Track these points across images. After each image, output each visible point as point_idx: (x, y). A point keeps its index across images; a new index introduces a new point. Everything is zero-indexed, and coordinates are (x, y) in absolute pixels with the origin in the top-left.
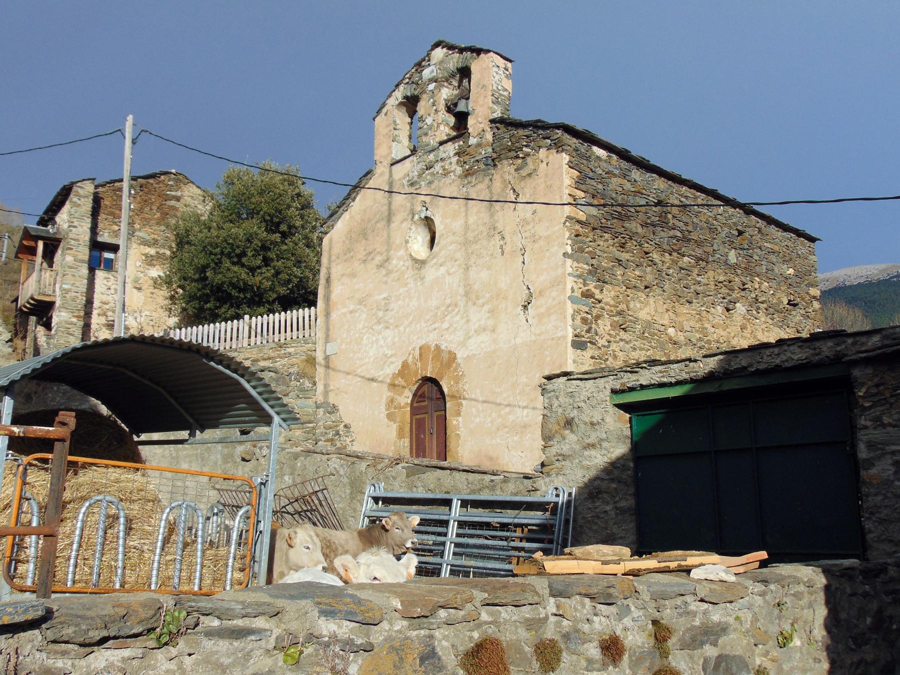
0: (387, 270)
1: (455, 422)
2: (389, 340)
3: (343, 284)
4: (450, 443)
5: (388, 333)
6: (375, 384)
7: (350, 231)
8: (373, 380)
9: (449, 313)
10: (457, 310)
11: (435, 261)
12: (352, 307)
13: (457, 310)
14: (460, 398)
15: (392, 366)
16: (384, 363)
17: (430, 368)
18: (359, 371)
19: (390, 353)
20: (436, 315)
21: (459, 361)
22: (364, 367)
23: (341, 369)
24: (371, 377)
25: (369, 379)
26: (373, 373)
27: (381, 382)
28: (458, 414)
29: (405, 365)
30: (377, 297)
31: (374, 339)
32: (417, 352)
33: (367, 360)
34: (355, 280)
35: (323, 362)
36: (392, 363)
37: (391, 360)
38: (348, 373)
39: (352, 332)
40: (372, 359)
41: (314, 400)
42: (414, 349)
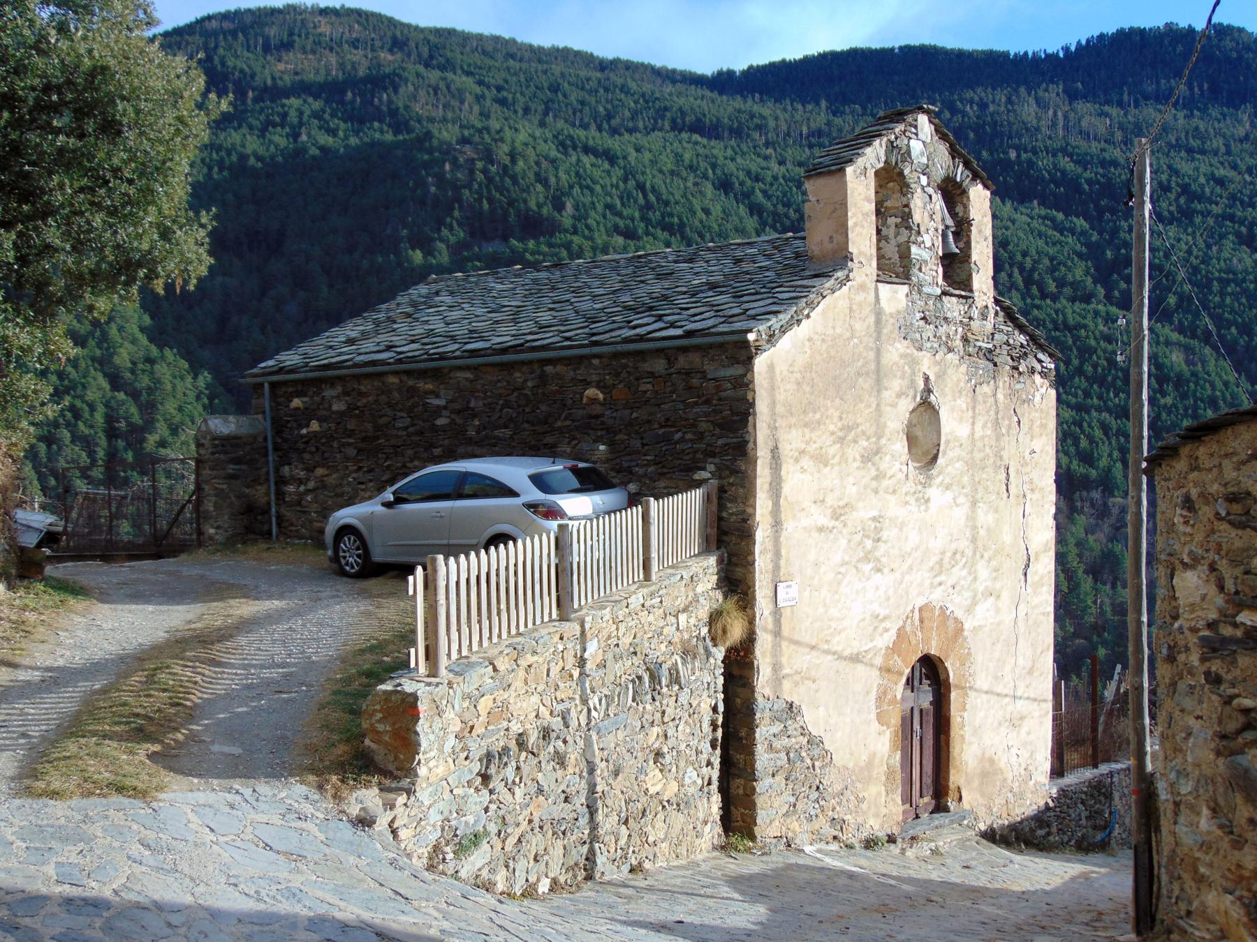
0: (878, 469)
1: (959, 719)
3: (803, 470)
11: (941, 478)
13: (964, 560)
15: (886, 635)
17: (934, 643)
20: (940, 563)
22: (843, 635)
29: (901, 633)
36: (886, 630)
37: (884, 625)
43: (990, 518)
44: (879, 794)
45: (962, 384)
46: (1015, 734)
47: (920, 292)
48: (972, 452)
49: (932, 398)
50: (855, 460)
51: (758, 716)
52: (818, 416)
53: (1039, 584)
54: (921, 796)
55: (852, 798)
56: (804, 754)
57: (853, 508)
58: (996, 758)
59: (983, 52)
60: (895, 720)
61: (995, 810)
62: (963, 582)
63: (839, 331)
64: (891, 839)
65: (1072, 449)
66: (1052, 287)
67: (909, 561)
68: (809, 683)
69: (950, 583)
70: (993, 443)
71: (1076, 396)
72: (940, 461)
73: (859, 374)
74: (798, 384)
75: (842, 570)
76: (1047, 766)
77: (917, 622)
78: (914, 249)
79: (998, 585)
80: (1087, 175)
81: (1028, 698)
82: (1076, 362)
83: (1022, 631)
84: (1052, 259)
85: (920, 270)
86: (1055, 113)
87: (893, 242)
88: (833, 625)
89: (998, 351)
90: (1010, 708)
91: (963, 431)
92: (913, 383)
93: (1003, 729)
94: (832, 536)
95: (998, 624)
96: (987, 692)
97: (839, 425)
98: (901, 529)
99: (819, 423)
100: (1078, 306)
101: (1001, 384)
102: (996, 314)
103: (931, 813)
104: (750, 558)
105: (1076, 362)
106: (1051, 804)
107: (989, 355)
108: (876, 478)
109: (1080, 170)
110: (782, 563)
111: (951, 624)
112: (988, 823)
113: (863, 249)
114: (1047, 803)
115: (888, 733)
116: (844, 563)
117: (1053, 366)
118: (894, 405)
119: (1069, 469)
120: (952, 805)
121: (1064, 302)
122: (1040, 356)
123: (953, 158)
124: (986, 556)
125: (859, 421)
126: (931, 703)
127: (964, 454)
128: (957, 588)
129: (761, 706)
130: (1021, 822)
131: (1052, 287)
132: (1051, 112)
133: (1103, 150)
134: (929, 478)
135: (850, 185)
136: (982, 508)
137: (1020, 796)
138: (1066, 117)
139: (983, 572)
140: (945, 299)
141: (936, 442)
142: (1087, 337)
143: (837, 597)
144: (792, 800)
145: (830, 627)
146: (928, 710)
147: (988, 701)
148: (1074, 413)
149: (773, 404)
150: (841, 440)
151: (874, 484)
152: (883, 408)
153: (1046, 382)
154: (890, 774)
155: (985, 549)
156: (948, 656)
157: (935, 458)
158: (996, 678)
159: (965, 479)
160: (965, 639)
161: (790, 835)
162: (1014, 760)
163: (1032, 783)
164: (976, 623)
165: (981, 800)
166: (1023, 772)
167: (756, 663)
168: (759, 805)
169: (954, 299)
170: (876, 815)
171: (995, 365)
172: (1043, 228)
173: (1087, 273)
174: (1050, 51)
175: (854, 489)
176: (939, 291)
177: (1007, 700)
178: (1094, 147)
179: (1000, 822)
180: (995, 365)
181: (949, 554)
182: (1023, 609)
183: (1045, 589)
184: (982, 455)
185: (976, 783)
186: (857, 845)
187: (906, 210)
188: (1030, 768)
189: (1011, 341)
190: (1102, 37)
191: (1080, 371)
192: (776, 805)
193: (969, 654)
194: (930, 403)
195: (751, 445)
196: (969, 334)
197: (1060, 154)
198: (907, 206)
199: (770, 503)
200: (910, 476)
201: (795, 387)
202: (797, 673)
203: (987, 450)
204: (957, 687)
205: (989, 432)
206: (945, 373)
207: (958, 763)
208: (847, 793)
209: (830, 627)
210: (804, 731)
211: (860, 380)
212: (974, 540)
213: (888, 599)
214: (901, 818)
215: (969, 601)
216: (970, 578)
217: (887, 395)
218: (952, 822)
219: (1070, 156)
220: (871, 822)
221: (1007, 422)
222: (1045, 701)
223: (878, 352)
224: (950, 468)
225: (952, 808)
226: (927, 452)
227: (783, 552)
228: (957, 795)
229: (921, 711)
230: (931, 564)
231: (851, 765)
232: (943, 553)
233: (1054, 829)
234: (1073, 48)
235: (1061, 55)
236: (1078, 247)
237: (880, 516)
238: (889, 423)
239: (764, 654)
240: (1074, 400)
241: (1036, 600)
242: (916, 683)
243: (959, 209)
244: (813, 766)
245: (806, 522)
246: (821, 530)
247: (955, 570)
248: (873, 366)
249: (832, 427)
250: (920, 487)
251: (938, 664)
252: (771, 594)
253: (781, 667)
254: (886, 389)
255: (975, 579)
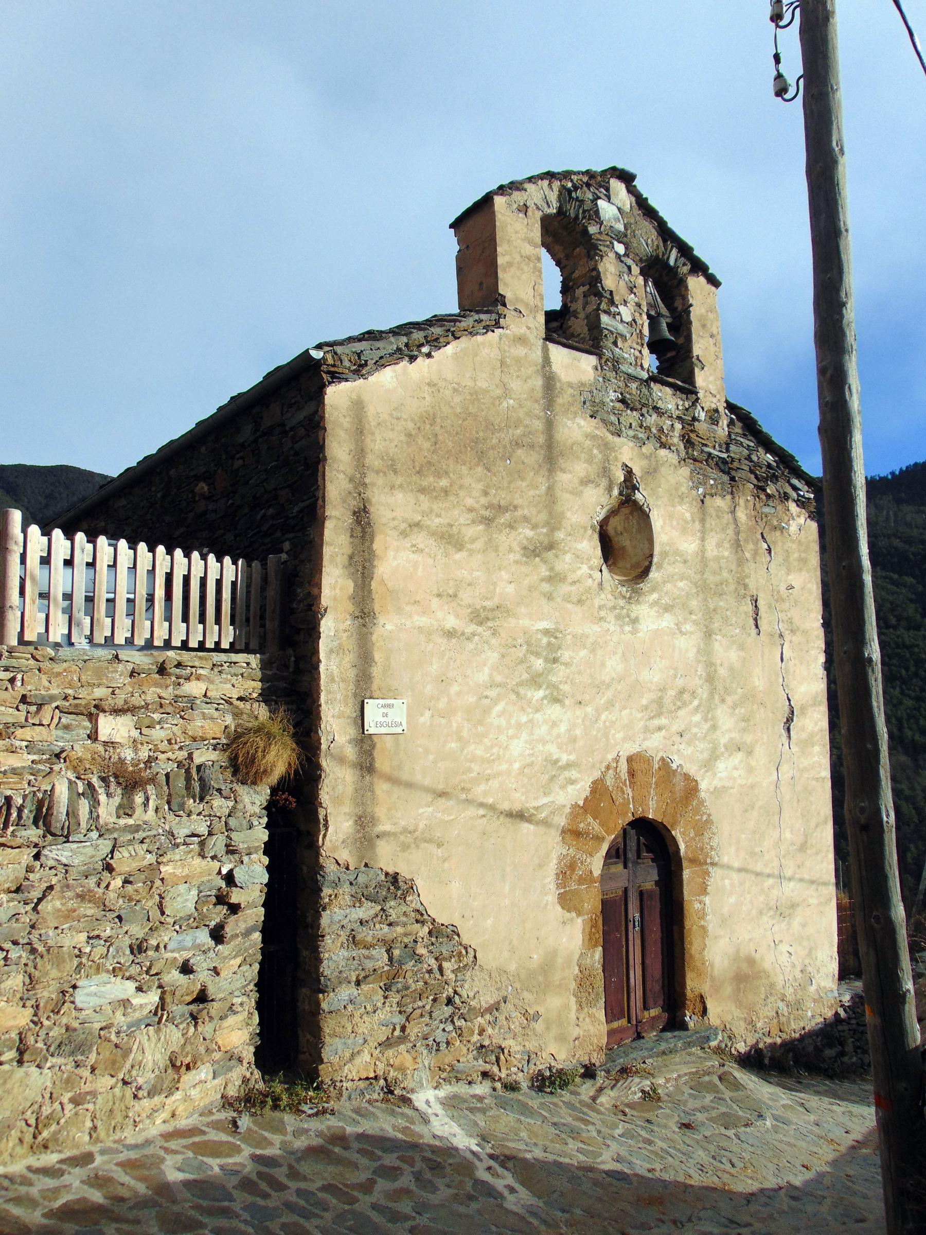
0: (552, 569)
1: (697, 906)
2: (563, 728)
3: (416, 549)
4: (691, 943)
5: (555, 711)
6: (526, 827)
7: (431, 418)
8: (520, 816)
9: (685, 704)
10: (696, 703)
11: (655, 596)
12: (451, 622)
13: (696, 703)
14: (706, 863)
15: (570, 789)
16: (553, 778)
17: (652, 804)
18: (479, 791)
19: (565, 758)
20: (659, 702)
21: (702, 795)
22: (495, 783)
23: (418, 778)
24: (517, 807)
25: (510, 815)
26: (518, 800)
27: (545, 823)
28: (704, 890)
29: (598, 788)
30: (525, 622)
31: (524, 719)
32: (623, 767)
33: (504, 767)
34: (458, 556)
35: (350, 752)
36: (572, 782)
37: (567, 774)
38: (442, 794)
39: (455, 689)
40: (517, 766)
41: (135, 1084)
42: (617, 760)
43: (734, 655)
44: (566, 1007)
45: (683, 489)
46: (783, 926)
47: (616, 369)
48: (702, 573)
49: (638, 496)
50: (511, 550)
51: (326, 891)
52: (444, 482)
53: (806, 744)
54: (646, 1007)
55: (515, 1014)
56: (421, 950)
57: (509, 613)
58: (757, 957)
59: (821, 440)
60: (592, 902)
61: (759, 1025)
62: (695, 730)
63: (484, 385)
64: (589, 1073)
65: (915, 726)
66: (893, 621)
67: (609, 694)
68: (432, 848)
69: (675, 728)
70: (733, 567)
71: (914, 691)
72: (654, 574)
73: (517, 444)
74: (409, 435)
75: (493, 693)
76: (833, 967)
77: (624, 775)
78: (604, 318)
79: (748, 738)
80: (913, 549)
81: (801, 880)
82: (913, 669)
83: (787, 797)
84: (892, 603)
85: (615, 343)
86: (888, 513)
87: (582, 315)
88: (476, 767)
89: (736, 464)
90: (775, 892)
91: (689, 546)
92: (605, 471)
93: (765, 919)
94: (471, 646)
95: (752, 786)
96: (740, 870)
97: (483, 501)
98: (593, 651)
99: (446, 492)
100: (912, 633)
101: (742, 502)
102: (731, 423)
103: (663, 1030)
104: (314, 659)
105: (913, 669)
106: (842, 1014)
107: (725, 466)
108: (550, 579)
109: (907, 547)
110: (376, 671)
111: (678, 781)
112: (751, 1041)
113: (522, 295)
114: (837, 1014)
115: (580, 920)
116: (492, 685)
117: (812, 496)
118: (576, 493)
119: (913, 740)
120: (691, 1020)
121: (902, 630)
122: (795, 482)
123: (665, 241)
124: (729, 700)
125: (518, 501)
126: (657, 883)
127: (691, 572)
128: (686, 737)
129: (331, 877)
130: (802, 1038)
131: (893, 621)
132: (885, 512)
133: (921, 534)
134: (637, 592)
135: (499, 216)
136: (719, 645)
137: (798, 1005)
138: (895, 515)
139: (726, 720)
140: (655, 387)
141: (647, 552)
142: (920, 653)
143: (480, 729)
144: (399, 1020)
145: (470, 770)
146: (651, 893)
147: (742, 884)
148: (914, 703)
149: (360, 453)
150: (488, 521)
151: (546, 587)
152: (558, 493)
153: (804, 514)
154: (584, 979)
155: (727, 691)
156: (675, 824)
157: (646, 571)
158: (752, 854)
159: (694, 603)
160: (702, 802)
161: (392, 1074)
162: (784, 959)
163: (812, 989)
164: (716, 783)
165: (737, 1013)
166: (799, 975)
167: (321, 813)
168: (327, 1030)
169: (668, 390)
170: (561, 1039)
171: (733, 479)
172: (885, 584)
173: (916, 611)
174: (882, 475)
175: (510, 589)
176: (645, 376)
177: (771, 881)
178: (915, 532)
179: (769, 1040)
180: (733, 479)
181: (671, 693)
182: (786, 771)
183: (817, 749)
184: (717, 578)
185: (728, 989)
186: (524, 1085)
187: (594, 273)
188: (810, 969)
189: (754, 458)
190: (916, 464)
191: (916, 675)
192: (363, 1029)
193: (709, 822)
194: (635, 503)
195: (320, 502)
196: (693, 436)
197: (893, 538)
198: (595, 269)
199: (350, 586)
200: (606, 585)
201: (403, 438)
202: (405, 831)
203: (725, 574)
204: (694, 861)
205: (726, 554)
206: (655, 470)
207: (698, 964)
208: (507, 1008)
209: (470, 770)
210: (421, 917)
211: (520, 452)
212: (710, 679)
213: (573, 740)
214: (604, 1041)
215: (706, 755)
216: (706, 726)
217: (563, 478)
218: (689, 1044)
219: (900, 538)
220: (553, 1048)
221: (751, 546)
222: (825, 884)
223: (550, 425)
224: (669, 586)
225: (691, 1025)
226: (638, 565)
227: (378, 656)
228: (699, 1006)
229: (641, 894)
230: (644, 702)
231: (512, 967)
232: (663, 690)
233: (849, 1048)
234: (897, 473)
235: (890, 477)
236: (909, 595)
237: (557, 630)
238: (569, 514)
239: (338, 800)
240: (913, 694)
241: (805, 762)
242: (631, 855)
243: (678, 303)
244: (441, 969)
245: (422, 621)
246: (450, 634)
247: (681, 713)
248: (541, 439)
249: (470, 502)
250: (621, 602)
251: (664, 832)
252: (350, 710)
253: (374, 821)
254: (563, 471)
255: (714, 727)
